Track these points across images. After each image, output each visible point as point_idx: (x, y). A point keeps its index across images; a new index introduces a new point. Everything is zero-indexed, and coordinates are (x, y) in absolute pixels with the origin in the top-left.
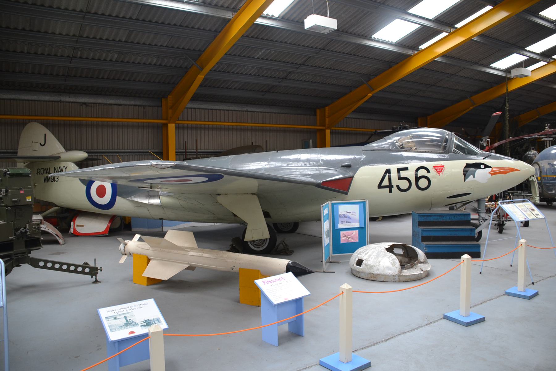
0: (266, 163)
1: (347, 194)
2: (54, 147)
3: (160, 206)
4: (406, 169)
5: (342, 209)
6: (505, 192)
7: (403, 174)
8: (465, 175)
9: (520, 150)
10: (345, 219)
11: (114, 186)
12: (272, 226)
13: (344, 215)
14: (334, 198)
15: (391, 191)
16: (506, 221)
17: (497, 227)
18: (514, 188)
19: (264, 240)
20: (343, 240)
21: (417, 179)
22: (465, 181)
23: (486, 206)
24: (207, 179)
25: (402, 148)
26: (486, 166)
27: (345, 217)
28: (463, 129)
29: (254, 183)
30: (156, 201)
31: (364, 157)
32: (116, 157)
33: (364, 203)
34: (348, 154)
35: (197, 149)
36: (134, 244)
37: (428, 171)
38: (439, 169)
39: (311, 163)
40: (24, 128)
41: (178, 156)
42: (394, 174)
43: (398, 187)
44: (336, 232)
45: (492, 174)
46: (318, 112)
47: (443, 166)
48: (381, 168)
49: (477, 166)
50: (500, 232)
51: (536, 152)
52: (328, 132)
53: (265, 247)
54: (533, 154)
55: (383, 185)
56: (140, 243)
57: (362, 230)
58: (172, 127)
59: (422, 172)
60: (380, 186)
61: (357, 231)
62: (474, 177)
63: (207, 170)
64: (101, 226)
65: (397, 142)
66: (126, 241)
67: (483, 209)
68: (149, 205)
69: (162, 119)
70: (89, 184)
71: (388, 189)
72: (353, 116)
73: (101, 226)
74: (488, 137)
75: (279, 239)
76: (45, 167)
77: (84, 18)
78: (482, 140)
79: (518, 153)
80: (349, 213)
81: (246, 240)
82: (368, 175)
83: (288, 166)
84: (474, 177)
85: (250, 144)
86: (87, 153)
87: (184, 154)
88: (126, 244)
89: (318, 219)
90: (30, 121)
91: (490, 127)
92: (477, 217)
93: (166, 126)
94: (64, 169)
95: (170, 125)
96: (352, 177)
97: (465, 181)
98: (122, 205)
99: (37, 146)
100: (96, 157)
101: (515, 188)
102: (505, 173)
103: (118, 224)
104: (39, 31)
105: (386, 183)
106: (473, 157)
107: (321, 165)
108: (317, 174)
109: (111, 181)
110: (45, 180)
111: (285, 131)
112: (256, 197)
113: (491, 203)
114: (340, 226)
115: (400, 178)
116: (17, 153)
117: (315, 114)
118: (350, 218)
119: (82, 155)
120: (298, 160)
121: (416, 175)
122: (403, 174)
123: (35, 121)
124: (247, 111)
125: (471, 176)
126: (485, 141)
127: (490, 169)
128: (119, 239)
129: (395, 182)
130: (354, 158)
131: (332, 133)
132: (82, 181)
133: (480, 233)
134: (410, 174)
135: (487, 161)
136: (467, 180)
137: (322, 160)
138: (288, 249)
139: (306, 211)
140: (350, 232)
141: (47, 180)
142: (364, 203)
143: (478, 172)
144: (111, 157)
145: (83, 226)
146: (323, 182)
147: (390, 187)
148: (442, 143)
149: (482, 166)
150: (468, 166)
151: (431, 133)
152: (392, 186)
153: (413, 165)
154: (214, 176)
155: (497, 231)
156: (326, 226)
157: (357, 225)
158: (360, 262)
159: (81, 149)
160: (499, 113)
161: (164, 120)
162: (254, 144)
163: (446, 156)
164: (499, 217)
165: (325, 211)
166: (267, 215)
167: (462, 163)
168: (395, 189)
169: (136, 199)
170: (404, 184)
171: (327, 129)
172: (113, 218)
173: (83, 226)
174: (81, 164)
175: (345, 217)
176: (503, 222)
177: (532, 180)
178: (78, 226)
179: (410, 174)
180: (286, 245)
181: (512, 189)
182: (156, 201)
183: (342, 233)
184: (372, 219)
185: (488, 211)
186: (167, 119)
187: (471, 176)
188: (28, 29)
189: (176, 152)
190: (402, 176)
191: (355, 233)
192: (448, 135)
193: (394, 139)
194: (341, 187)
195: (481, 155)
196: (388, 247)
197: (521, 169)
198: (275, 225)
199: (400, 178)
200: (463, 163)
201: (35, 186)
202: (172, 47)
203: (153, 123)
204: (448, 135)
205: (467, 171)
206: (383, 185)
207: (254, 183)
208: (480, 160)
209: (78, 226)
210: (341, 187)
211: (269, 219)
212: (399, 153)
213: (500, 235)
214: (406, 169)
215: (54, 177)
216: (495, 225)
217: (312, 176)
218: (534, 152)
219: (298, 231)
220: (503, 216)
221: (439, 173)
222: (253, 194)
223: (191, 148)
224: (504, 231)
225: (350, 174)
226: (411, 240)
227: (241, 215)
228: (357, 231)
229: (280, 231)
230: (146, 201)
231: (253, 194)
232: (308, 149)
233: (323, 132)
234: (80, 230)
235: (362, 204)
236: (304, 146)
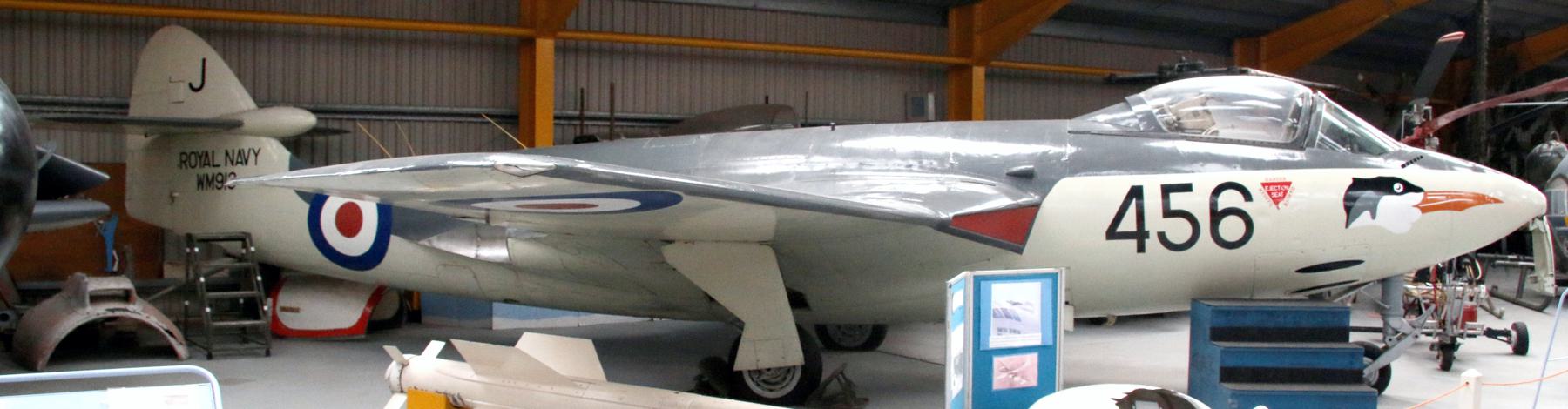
0: (800, 158)
1: (1020, 251)
2: (228, 94)
3: (508, 266)
4: (1187, 188)
5: (1001, 295)
6: (1459, 259)
7: (1178, 201)
8: (1348, 209)
9: (1524, 137)
10: (1007, 323)
11: (384, 211)
12: (814, 334)
13: (1005, 310)
14: (986, 262)
15: (1141, 249)
16: (1461, 335)
17: (1435, 353)
18: (1498, 243)
20: (999, 381)
21: (1216, 216)
22: (1347, 225)
23: (1408, 294)
24: (637, 204)
25: (1177, 129)
26: (1409, 188)
27: (1008, 316)
28: (1361, 77)
29: (767, 217)
30: (497, 252)
31: (1070, 150)
32: (392, 125)
33: (1054, 277)
34: (1027, 139)
35: (612, 111)
36: (427, 366)
37: (1247, 196)
38: (1278, 192)
39: (925, 162)
40: (147, 40)
41: (559, 129)
42: (1153, 201)
43: (1162, 237)
44: (982, 359)
45: (1424, 210)
46: (953, 17)
47: (1289, 184)
48: (1116, 186)
49: (1384, 185)
50: (1446, 366)
51: (1562, 145)
53: (794, 383)
54: (1555, 152)
55: (1121, 228)
56: (447, 364)
57: (1046, 353)
59: (1229, 199)
60: (1112, 233)
62: (1374, 216)
63: (637, 183)
64: (344, 313)
65: (1162, 111)
66: (407, 357)
67: (1398, 302)
68: (477, 261)
69: (520, 25)
70: (316, 201)
71: (1133, 243)
72: (1053, 29)
73: (344, 313)
74: (1426, 100)
75: (831, 364)
76: (199, 149)
78: (1410, 109)
79: (1509, 150)
80: (1019, 304)
81: (738, 366)
82: (1080, 204)
83: (859, 169)
84: (1374, 216)
85: (762, 101)
86: (314, 111)
87: (580, 131)
88: (404, 365)
89: (937, 317)
90: (164, 22)
91: (1433, 71)
92: (1379, 324)
93: (529, 43)
94: (252, 155)
97: (1347, 225)
98: (406, 260)
100: (336, 126)
101: (1504, 246)
102: (1460, 207)
103: (389, 309)
105: (1129, 223)
106: (1373, 160)
107: (952, 170)
108: (940, 194)
109: (377, 199)
110: (200, 183)
111: (860, 67)
112: (769, 253)
113: (1422, 286)
114: (995, 341)
115: (1168, 213)
116: (127, 106)
117: (944, 22)
118: (1018, 319)
119: (303, 119)
120: (887, 155)
121: (1213, 205)
122: (1178, 201)
123: (178, 24)
125: (1366, 214)
126: (1418, 110)
127: (1418, 197)
128: (387, 348)
130: (1045, 154)
131: (990, 76)
132: (303, 195)
133: (1385, 373)
135: (1413, 174)
136: (1353, 225)
137: (956, 156)
138: (853, 394)
139: (908, 293)
140: (1015, 358)
142: (1054, 277)
143: (1386, 201)
144: (378, 125)
145: (296, 310)
146: (955, 217)
147: (1140, 235)
148: (1284, 119)
150: (1358, 184)
151: (1265, 88)
152: (1146, 235)
153: (1204, 179)
154: (656, 198)
155: (1437, 365)
156: (957, 340)
157: (1035, 339)
159: (298, 104)
160: (1458, 35)
161: (525, 27)
162: (771, 101)
163: (1299, 156)
164: (1442, 324)
165: (958, 297)
166: (797, 301)
167: (1342, 178)
168: (1152, 243)
170: (1179, 230)
171: (979, 64)
172: (378, 294)
173: (296, 310)
174: (303, 149)
175: (1008, 316)
176: (1454, 339)
177: (1538, 231)
178: (284, 309)
180: (849, 383)
181: (1495, 248)
182: (497, 252)
183: (998, 361)
184: (1090, 323)
185: (1413, 307)
186: (532, 25)
187: (1366, 214)
189: (556, 118)
191: (1031, 360)
192: (1302, 97)
193: (1154, 99)
194: (1008, 232)
195: (1398, 155)
196: (1121, 396)
197: (1512, 198)
198: (822, 330)
199: (1168, 213)
200: (1345, 177)
201: (173, 198)
203: (494, 35)
204: (1302, 97)
205: (1355, 199)
206: (1121, 228)
207: (768, 215)
208: (1390, 168)
209: (284, 309)
210: (1008, 232)
211: (802, 312)
212: (1167, 145)
213: (1445, 375)
214: (1187, 188)
216: (1432, 347)
217: (928, 200)
218: (1557, 144)
219: (881, 347)
220: (1455, 323)
221: (1276, 201)
222: (762, 243)
223: (597, 106)
224: (1455, 365)
225: (1028, 198)
226: (1183, 381)
227: (729, 299)
229: (832, 345)
230: (469, 251)
231: (762, 243)
232: (919, 126)
233: (963, 71)
234: (290, 321)
236: (913, 113)
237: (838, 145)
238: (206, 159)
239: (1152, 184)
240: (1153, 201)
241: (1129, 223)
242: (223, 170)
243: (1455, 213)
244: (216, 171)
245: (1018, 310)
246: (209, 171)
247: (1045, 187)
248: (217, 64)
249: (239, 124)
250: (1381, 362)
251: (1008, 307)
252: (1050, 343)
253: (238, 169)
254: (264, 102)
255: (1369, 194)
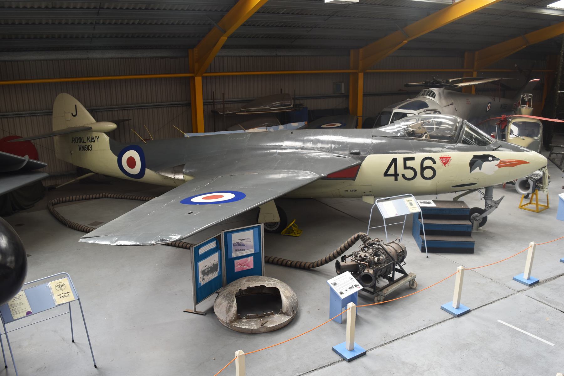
1: (354, 180)
2: (86, 118)
4: (413, 159)
7: (409, 163)
10: (239, 248)
13: (238, 243)
15: (396, 179)
19: (276, 223)
21: (423, 169)
26: (494, 158)
37: (434, 162)
42: (400, 163)
43: (403, 176)
45: (499, 167)
47: (450, 158)
48: (387, 158)
49: (485, 158)
52: (361, 75)
55: (388, 173)
58: (198, 80)
59: (428, 163)
60: (386, 174)
61: (252, 257)
62: (480, 169)
68: (174, 179)
71: (393, 178)
77: (98, 14)
84: (480, 169)
94: (96, 139)
95: (196, 78)
96: (359, 165)
99: (70, 116)
104: (61, 8)
105: (392, 171)
110: (80, 148)
118: (244, 245)
122: (409, 163)
124: (276, 56)
125: (478, 168)
129: (401, 170)
134: (416, 164)
136: (473, 172)
140: (243, 259)
141: (82, 148)
143: (485, 164)
147: (396, 175)
149: (490, 158)
150: (475, 157)
152: (398, 175)
157: (252, 251)
158: (335, 284)
162: (283, 92)
167: (469, 155)
168: (400, 178)
169: (163, 174)
179: (416, 164)
186: (193, 72)
187: (478, 168)
188: (50, 7)
190: (408, 166)
191: (251, 259)
199: (406, 167)
202: (193, 10)
206: (388, 173)
214: (413, 159)
215: (88, 146)
221: (445, 164)
228: (252, 257)
235: (257, 229)
237: (306, 138)
238: (81, 140)
239: (400, 158)
240: (400, 163)
241: (392, 171)
242: (87, 144)
243: (511, 167)
244: (85, 144)
245: (244, 242)
246: (81, 144)
247: (363, 159)
248: (81, 107)
249: (91, 128)
250: (484, 215)
251: (239, 241)
252: (258, 251)
253: (92, 143)
254: (98, 120)
255: (479, 161)
